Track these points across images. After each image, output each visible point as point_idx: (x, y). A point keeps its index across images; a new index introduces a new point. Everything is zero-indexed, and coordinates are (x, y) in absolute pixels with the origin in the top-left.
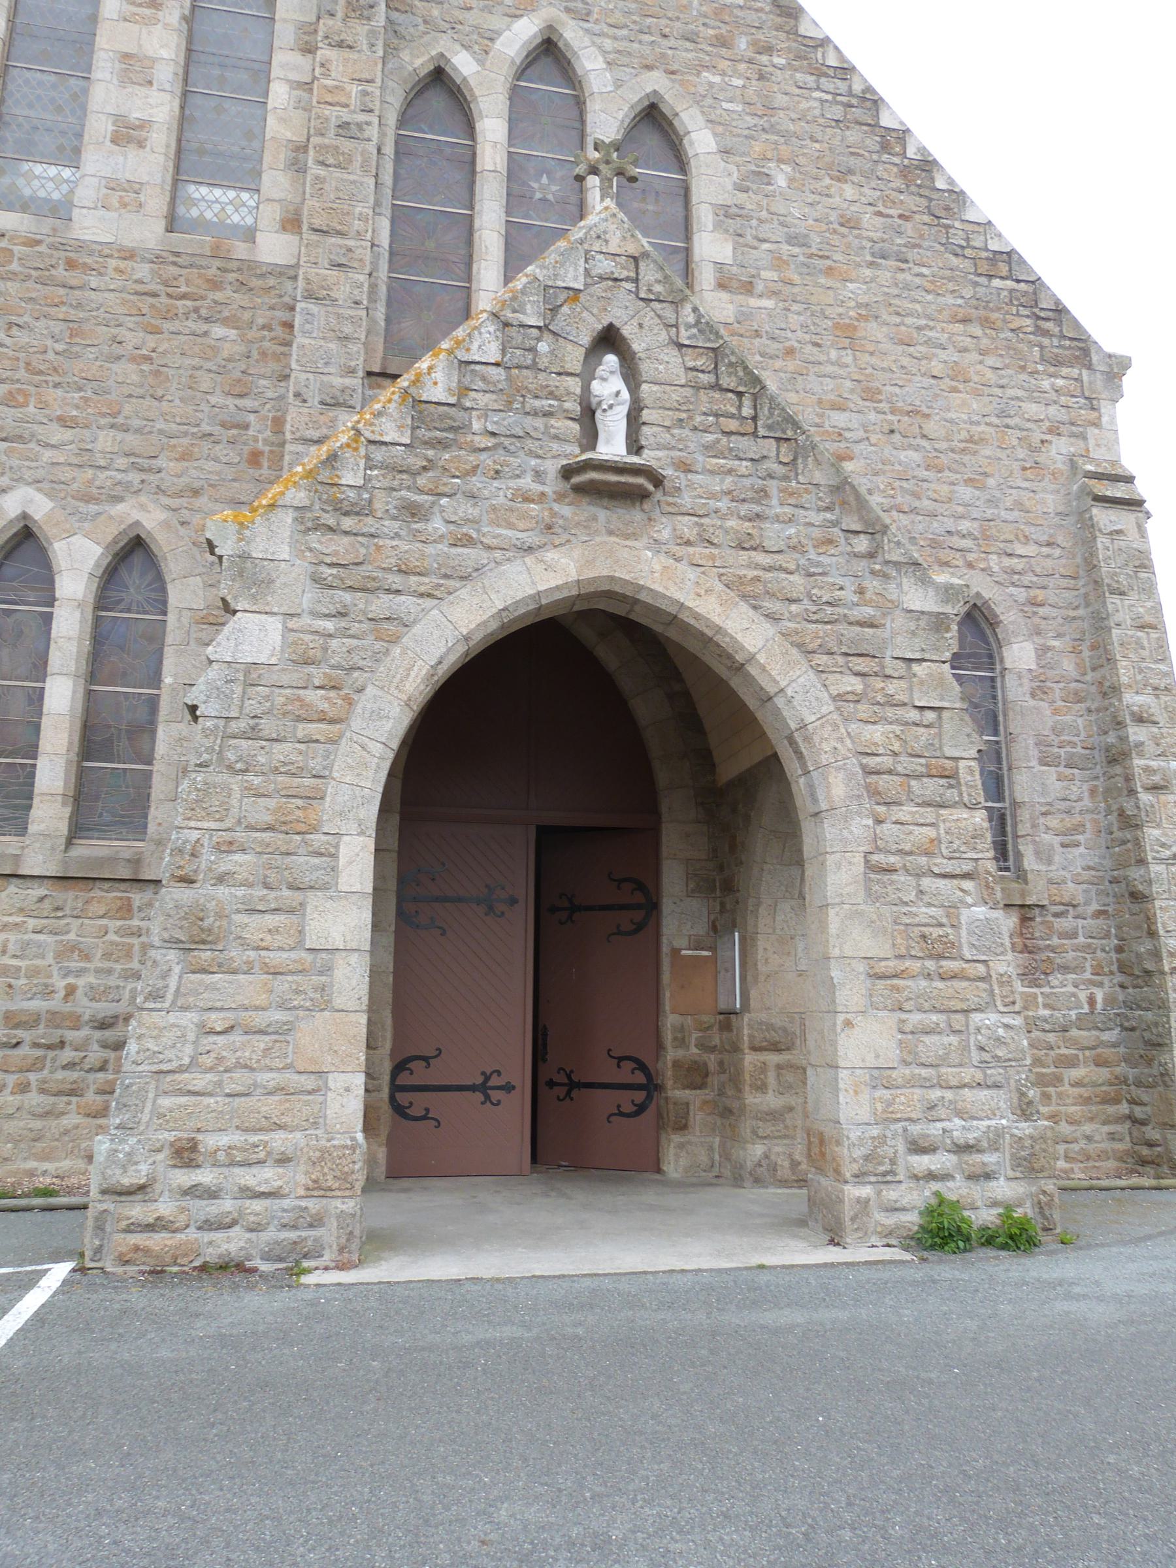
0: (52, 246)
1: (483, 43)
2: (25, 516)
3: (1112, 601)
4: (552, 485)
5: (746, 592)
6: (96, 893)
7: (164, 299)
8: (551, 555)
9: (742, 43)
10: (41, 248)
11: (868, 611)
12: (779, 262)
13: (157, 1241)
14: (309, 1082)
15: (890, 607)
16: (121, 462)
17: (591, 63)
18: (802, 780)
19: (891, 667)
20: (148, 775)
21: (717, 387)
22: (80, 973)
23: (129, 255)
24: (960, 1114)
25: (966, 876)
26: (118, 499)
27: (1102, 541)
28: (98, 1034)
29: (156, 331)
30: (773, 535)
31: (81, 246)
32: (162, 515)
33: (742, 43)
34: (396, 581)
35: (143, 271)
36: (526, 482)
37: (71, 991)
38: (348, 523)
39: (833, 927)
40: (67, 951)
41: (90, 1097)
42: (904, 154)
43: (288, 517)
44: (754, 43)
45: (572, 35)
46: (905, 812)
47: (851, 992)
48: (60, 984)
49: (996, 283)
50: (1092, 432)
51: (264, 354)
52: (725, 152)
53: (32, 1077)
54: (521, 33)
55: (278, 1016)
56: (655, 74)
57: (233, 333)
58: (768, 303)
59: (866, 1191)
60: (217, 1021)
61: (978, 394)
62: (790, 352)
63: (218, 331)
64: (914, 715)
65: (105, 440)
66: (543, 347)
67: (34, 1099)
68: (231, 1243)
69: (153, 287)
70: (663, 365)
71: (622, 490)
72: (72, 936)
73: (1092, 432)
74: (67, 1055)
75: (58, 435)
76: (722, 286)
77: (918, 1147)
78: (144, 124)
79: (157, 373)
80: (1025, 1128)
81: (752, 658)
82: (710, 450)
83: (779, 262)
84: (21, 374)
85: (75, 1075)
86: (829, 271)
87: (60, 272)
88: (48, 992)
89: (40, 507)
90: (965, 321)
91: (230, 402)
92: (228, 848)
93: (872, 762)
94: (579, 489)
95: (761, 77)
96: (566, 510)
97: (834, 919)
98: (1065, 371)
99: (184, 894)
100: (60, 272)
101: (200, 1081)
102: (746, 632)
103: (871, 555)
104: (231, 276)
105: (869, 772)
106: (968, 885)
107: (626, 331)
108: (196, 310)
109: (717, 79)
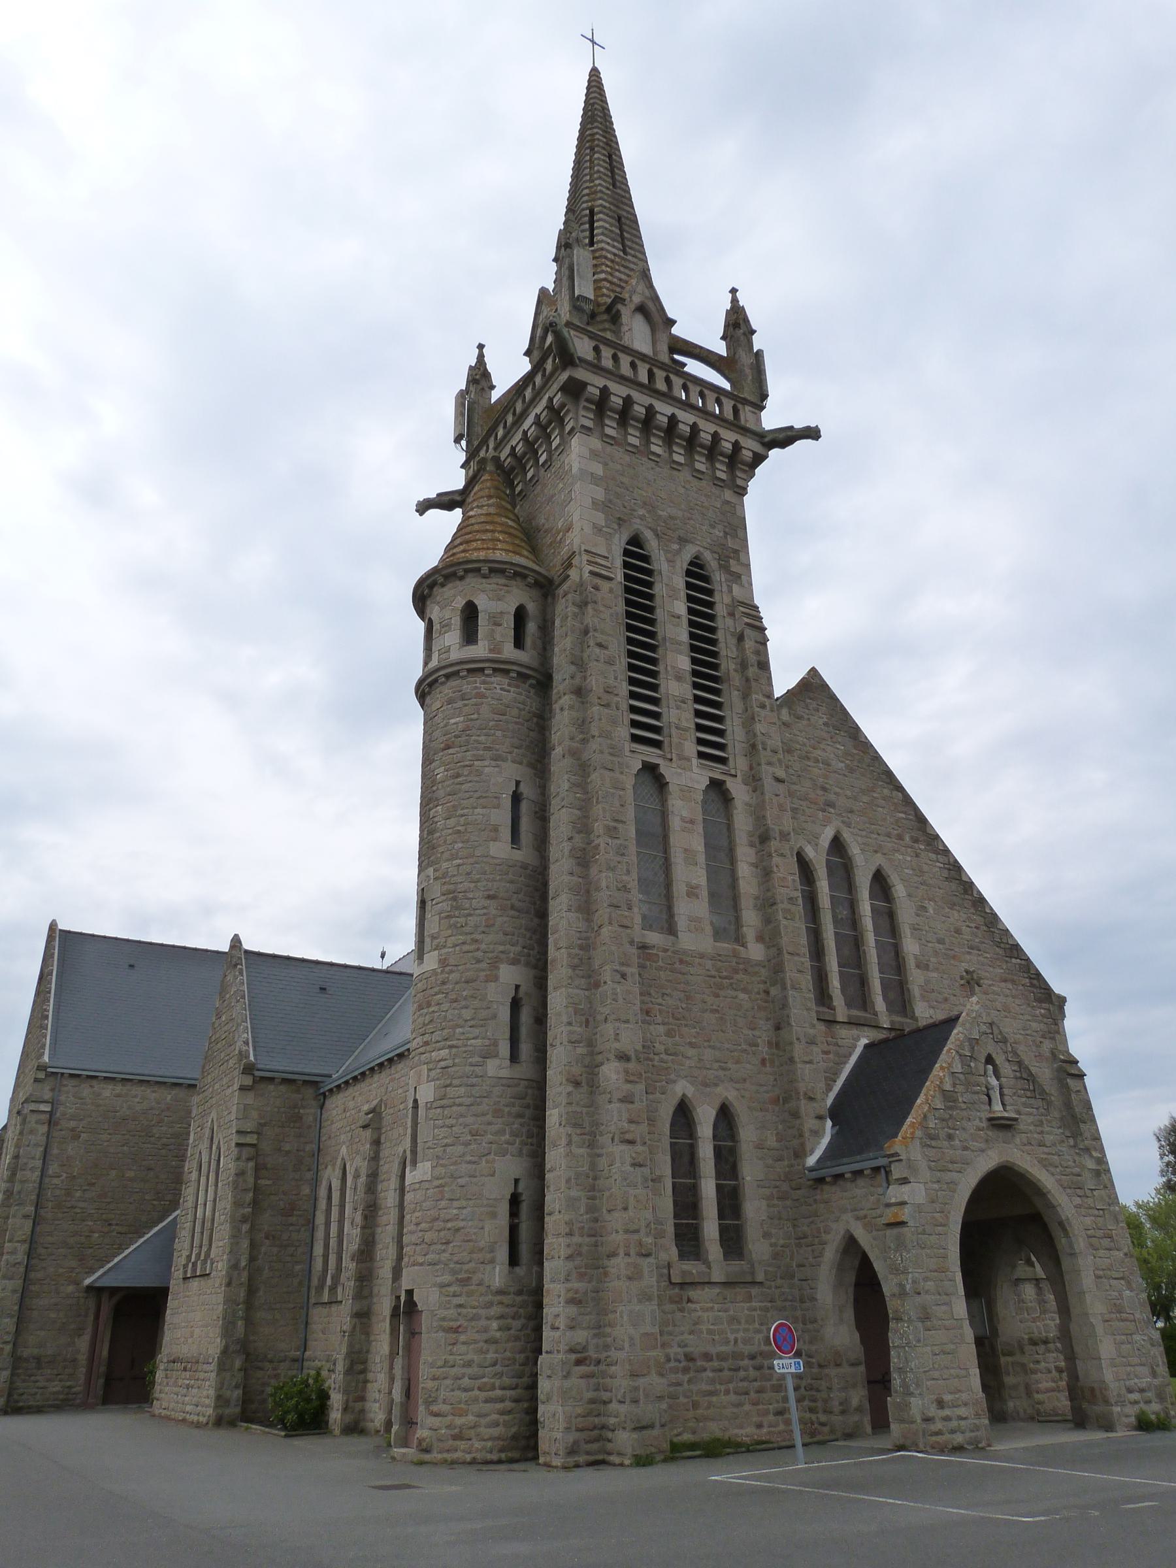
0: (673, 952)
1: (814, 839)
2: (684, 1095)
3: (1082, 1125)
4: (984, 1124)
5: (1045, 1164)
6: (738, 1290)
7: (718, 979)
8: (989, 1153)
9: (907, 838)
10: (669, 953)
11: (1077, 1170)
12: (936, 953)
13: (938, 1439)
14: (963, 1372)
15: (1083, 1167)
16: (716, 1066)
17: (855, 850)
18: (1063, 1240)
19: (1089, 1193)
20: (676, 1217)
21: (1021, 1078)
22: (738, 1331)
23: (702, 956)
24: (1136, 1376)
25: (1122, 1278)
26: (716, 1085)
27: (1073, 1096)
28: (751, 1362)
29: (717, 996)
30: (1049, 1139)
31: (685, 952)
32: (735, 1093)
33: (907, 838)
34: (950, 1166)
35: (709, 964)
36: (977, 1122)
37: (736, 1341)
38: (933, 1143)
39: (1088, 1301)
40: (733, 1320)
41: (753, 1395)
42: (972, 895)
43: (918, 1142)
44: (912, 838)
45: (846, 835)
46: (1102, 1253)
47: (1100, 1329)
48: (732, 1337)
49: (1014, 960)
50: (1057, 1036)
51: (759, 1008)
52: (909, 895)
53: (731, 1386)
54: (828, 834)
55: (952, 1347)
56: (879, 855)
57: (746, 996)
58: (935, 975)
59: (1119, 1409)
60: (937, 1349)
61: (1015, 1018)
62: (946, 1000)
63: (742, 996)
64: (1096, 1212)
65: (708, 1054)
66: (972, 1064)
67: (732, 1397)
68: (959, 1439)
69: (713, 973)
70: (1007, 1069)
71: (1002, 1126)
72: (731, 1313)
73: (1057, 1036)
74: (742, 1374)
75: (691, 1052)
76: (918, 966)
77: (1130, 1391)
78: (697, 887)
79: (722, 1018)
80: (1156, 1382)
81: (1049, 1192)
82: (1025, 1105)
83: (936, 953)
84: (671, 1020)
85: (745, 1384)
86: (954, 957)
87: (677, 965)
88: (727, 1342)
89: (690, 1091)
90: (1005, 981)
91: (750, 1032)
92: (926, 1279)
93: (1089, 1232)
94: (993, 1125)
95: (917, 856)
96: (990, 1133)
97: (1088, 1298)
98: (1044, 1005)
99: (918, 1299)
100: (677, 965)
101: (936, 1374)
102: (1046, 1179)
103: (1075, 1146)
104: (741, 966)
105: (1089, 1237)
106: (1122, 1282)
107: (994, 1056)
108: (731, 984)
109: (901, 857)
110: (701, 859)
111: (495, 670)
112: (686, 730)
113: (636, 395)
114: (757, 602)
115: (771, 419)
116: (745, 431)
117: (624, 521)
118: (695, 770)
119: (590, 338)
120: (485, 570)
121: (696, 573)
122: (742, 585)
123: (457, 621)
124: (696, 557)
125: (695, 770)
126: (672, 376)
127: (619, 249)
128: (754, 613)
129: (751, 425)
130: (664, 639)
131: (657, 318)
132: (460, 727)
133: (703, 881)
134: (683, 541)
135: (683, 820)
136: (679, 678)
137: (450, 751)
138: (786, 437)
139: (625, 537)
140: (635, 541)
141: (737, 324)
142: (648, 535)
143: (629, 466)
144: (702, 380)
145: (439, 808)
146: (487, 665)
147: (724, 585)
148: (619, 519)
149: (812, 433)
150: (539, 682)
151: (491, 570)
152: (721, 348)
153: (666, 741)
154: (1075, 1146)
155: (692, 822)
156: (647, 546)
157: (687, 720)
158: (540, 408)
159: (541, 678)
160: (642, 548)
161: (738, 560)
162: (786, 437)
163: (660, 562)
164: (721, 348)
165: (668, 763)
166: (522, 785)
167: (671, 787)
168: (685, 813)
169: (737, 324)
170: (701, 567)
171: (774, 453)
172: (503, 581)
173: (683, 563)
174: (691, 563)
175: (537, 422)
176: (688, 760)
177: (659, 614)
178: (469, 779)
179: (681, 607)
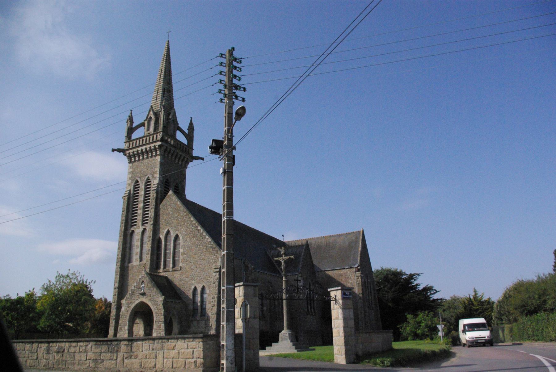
115: (195, 154)
138: (197, 158)
141: (191, 127)
149: (203, 159)
152: (187, 131)
162: (197, 158)
164: (187, 131)
169: (191, 127)
171: (194, 161)
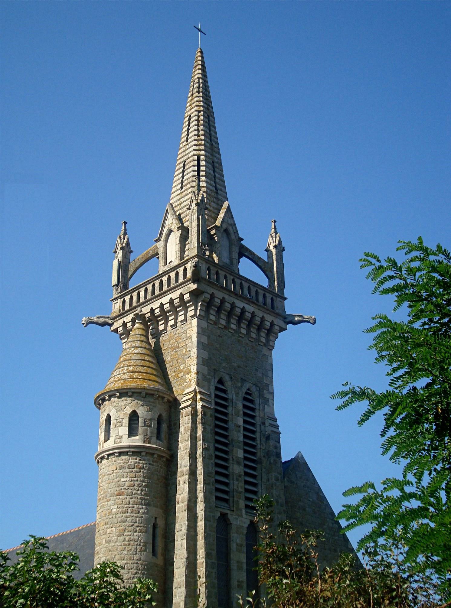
78: (242, 582)
103: (215, 323)
110: (245, 566)
111: (146, 453)
112: (240, 493)
113: (226, 297)
114: (276, 415)
116: (278, 315)
117: (217, 371)
118: (244, 516)
119: (206, 262)
120: (144, 394)
121: (248, 399)
122: (269, 406)
123: (126, 421)
124: (248, 389)
125: (244, 516)
126: (243, 282)
127: (213, 186)
128: (274, 423)
129: (280, 312)
130: (233, 440)
131: (233, 236)
132: (127, 484)
133: (245, 579)
134: (243, 381)
135: (237, 545)
136: (238, 463)
137: (121, 497)
139: (216, 380)
140: (221, 381)
142: (227, 378)
143: (219, 336)
144: (257, 284)
145: (114, 529)
146: (143, 450)
147: (261, 406)
148: (214, 369)
150: (167, 460)
151: (147, 394)
153: (231, 499)
154: (215, 323)
155: (241, 545)
156: (226, 384)
157: (241, 487)
158: (175, 295)
159: (168, 457)
160: (223, 385)
161: (268, 390)
163: (231, 395)
165: (232, 513)
166: (158, 519)
167: (234, 527)
168: (238, 541)
170: (250, 394)
172: (152, 400)
173: (242, 395)
174: (247, 393)
175: (171, 301)
176: (241, 510)
177: (230, 425)
178: (132, 514)
179: (240, 421)
